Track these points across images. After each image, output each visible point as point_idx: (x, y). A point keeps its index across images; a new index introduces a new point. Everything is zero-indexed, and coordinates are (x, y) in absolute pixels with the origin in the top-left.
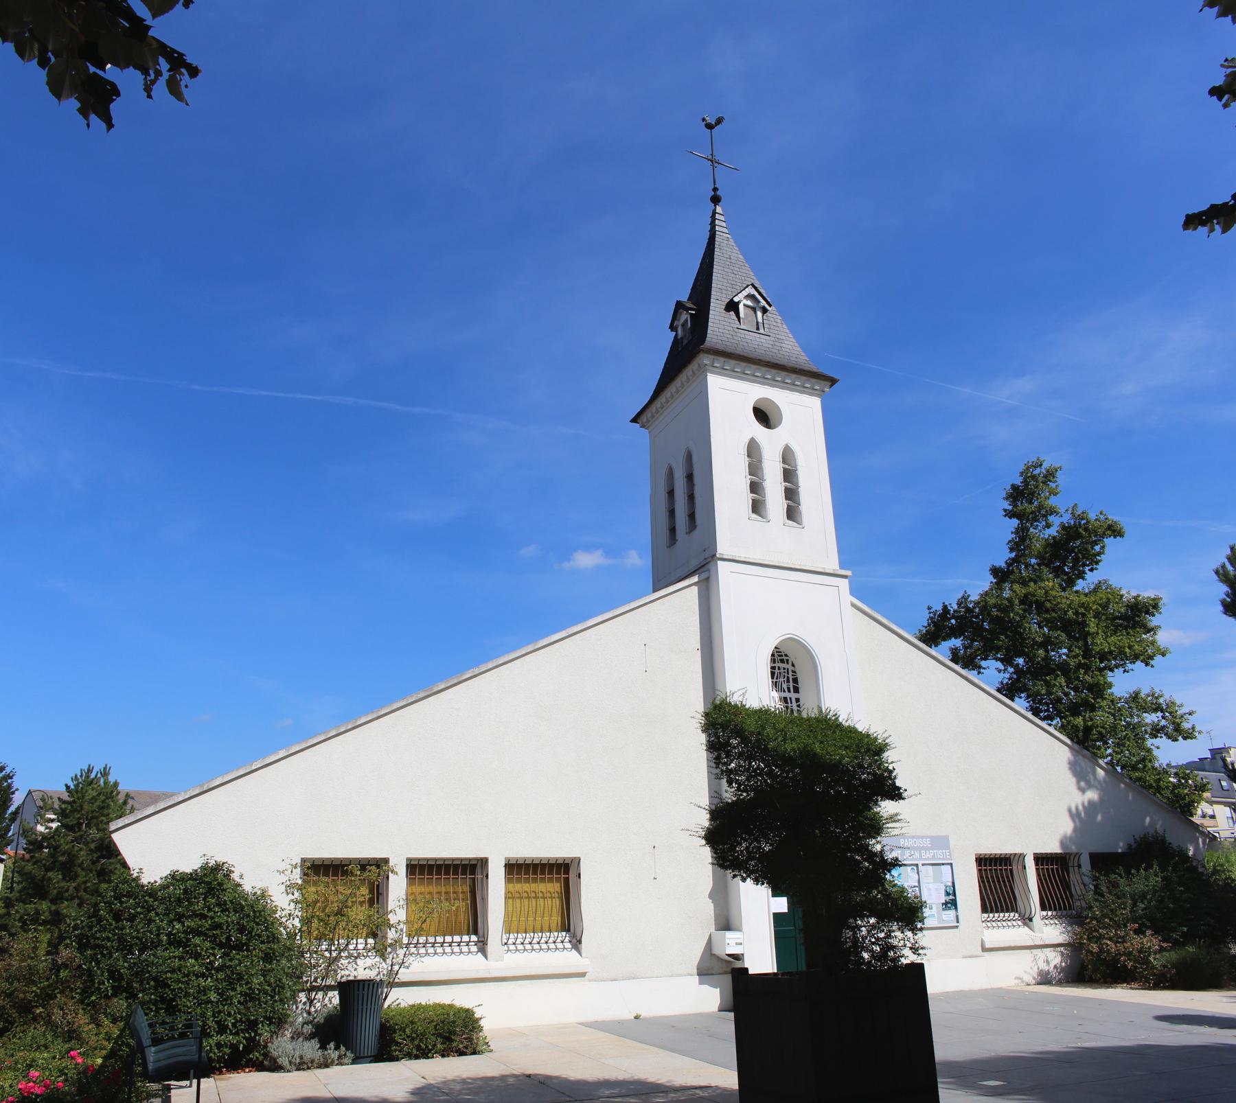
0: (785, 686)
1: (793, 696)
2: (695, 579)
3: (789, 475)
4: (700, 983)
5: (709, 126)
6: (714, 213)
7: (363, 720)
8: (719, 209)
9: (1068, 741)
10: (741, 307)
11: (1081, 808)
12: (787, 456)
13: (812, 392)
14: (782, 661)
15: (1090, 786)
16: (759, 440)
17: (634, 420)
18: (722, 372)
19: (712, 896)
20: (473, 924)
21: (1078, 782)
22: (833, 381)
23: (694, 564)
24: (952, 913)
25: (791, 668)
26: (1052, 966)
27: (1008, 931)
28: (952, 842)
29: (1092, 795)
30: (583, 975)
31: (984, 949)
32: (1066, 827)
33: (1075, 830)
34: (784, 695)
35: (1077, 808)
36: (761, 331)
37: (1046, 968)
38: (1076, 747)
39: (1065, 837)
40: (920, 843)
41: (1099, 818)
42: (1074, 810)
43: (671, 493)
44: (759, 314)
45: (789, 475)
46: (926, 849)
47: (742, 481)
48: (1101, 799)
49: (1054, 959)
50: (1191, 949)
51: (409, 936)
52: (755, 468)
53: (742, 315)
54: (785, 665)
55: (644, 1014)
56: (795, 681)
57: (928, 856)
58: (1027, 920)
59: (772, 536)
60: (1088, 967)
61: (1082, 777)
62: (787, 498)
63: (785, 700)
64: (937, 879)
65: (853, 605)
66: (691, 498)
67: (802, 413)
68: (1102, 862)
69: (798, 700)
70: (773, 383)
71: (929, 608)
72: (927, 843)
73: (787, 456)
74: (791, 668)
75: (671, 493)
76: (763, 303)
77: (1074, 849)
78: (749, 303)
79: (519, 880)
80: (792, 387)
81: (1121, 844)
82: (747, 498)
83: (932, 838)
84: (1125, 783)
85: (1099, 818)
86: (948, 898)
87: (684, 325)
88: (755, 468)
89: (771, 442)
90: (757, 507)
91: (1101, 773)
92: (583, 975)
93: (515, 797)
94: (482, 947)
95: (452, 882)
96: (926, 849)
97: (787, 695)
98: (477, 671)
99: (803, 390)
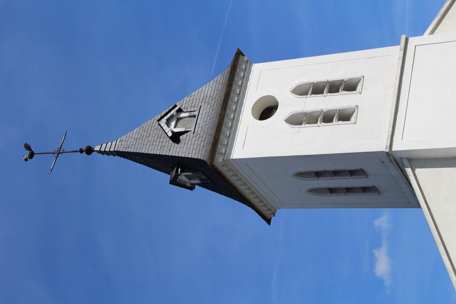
2: (409, 171)
3: (317, 89)
5: (32, 155)
6: (100, 152)
8: (97, 148)
10: (176, 130)
12: (301, 91)
13: (248, 71)
17: (269, 221)
18: (229, 146)
22: (239, 54)
23: (395, 172)
36: (196, 113)
43: (332, 191)
44: (183, 115)
45: (317, 89)
47: (323, 129)
52: (310, 119)
53: (183, 130)
62: (337, 91)
66: (336, 173)
67: (266, 79)
70: (239, 103)
73: (301, 91)
75: (332, 191)
76: (173, 112)
78: (173, 124)
80: (244, 87)
87: (190, 178)
88: (310, 119)
89: (289, 104)
90: (345, 116)
99: (246, 79)
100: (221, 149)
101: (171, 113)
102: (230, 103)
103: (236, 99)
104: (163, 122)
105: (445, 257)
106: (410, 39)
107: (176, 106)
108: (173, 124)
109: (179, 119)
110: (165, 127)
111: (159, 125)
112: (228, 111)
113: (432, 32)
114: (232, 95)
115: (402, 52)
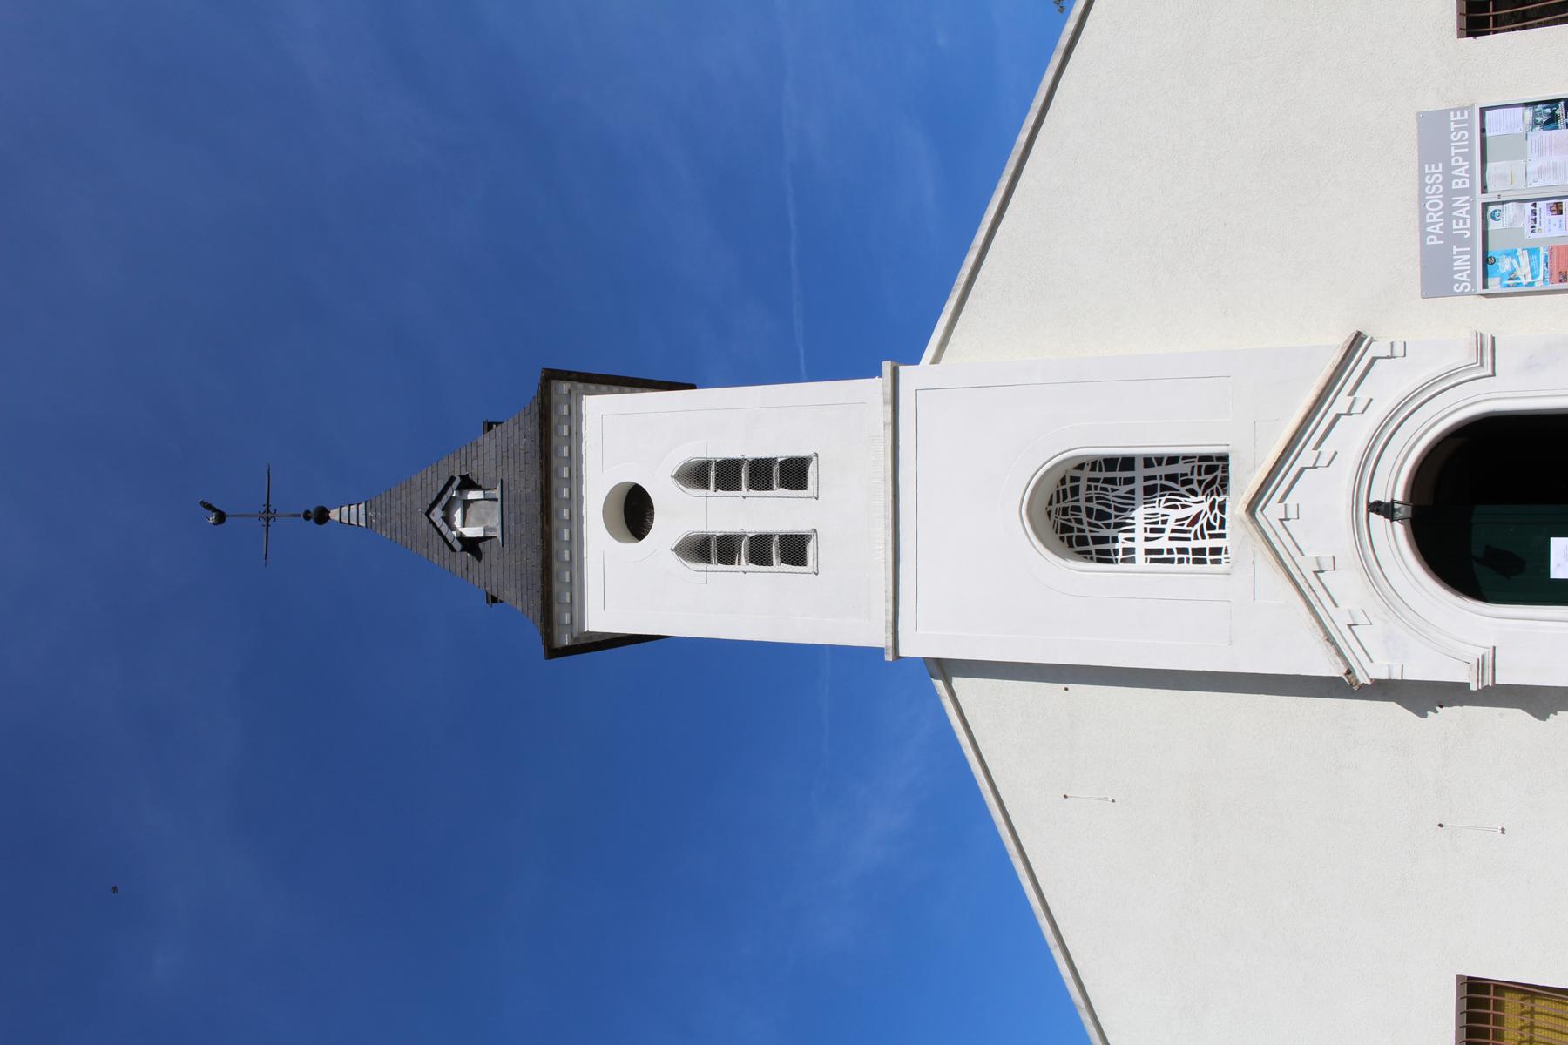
0: (1123, 490)
1: (1140, 472)
5: (221, 517)
12: (696, 475)
13: (575, 418)
14: (1075, 491)
16: (675, 540)
25: (1086, 474)
28: (1431, 104)
34: (1139, 494)
40: (1435, 193)
44: (472, 495)
46: (1448, 177)
47: (744, 577)
54: (1083, 484)
57: (1465, 172)
63: (1149, 491)
64: (1517, 149)
65: (936, 360)
67: (622, 438)
69: (1148, 462)
72: (1435, 171)
73: (696, 475)
74: (1086, 474)
80: (575, 479)
82: (779, 573)
90: (794, 549)
96: (1448, 177)
97: (1139, 486)
99: (575, 437)
102: (555, 504)
103: (566, 491)
105: (1023, 137)
106: (903, 369)
108: (458, 515)
111: (432, 522)
115: (890, 408)
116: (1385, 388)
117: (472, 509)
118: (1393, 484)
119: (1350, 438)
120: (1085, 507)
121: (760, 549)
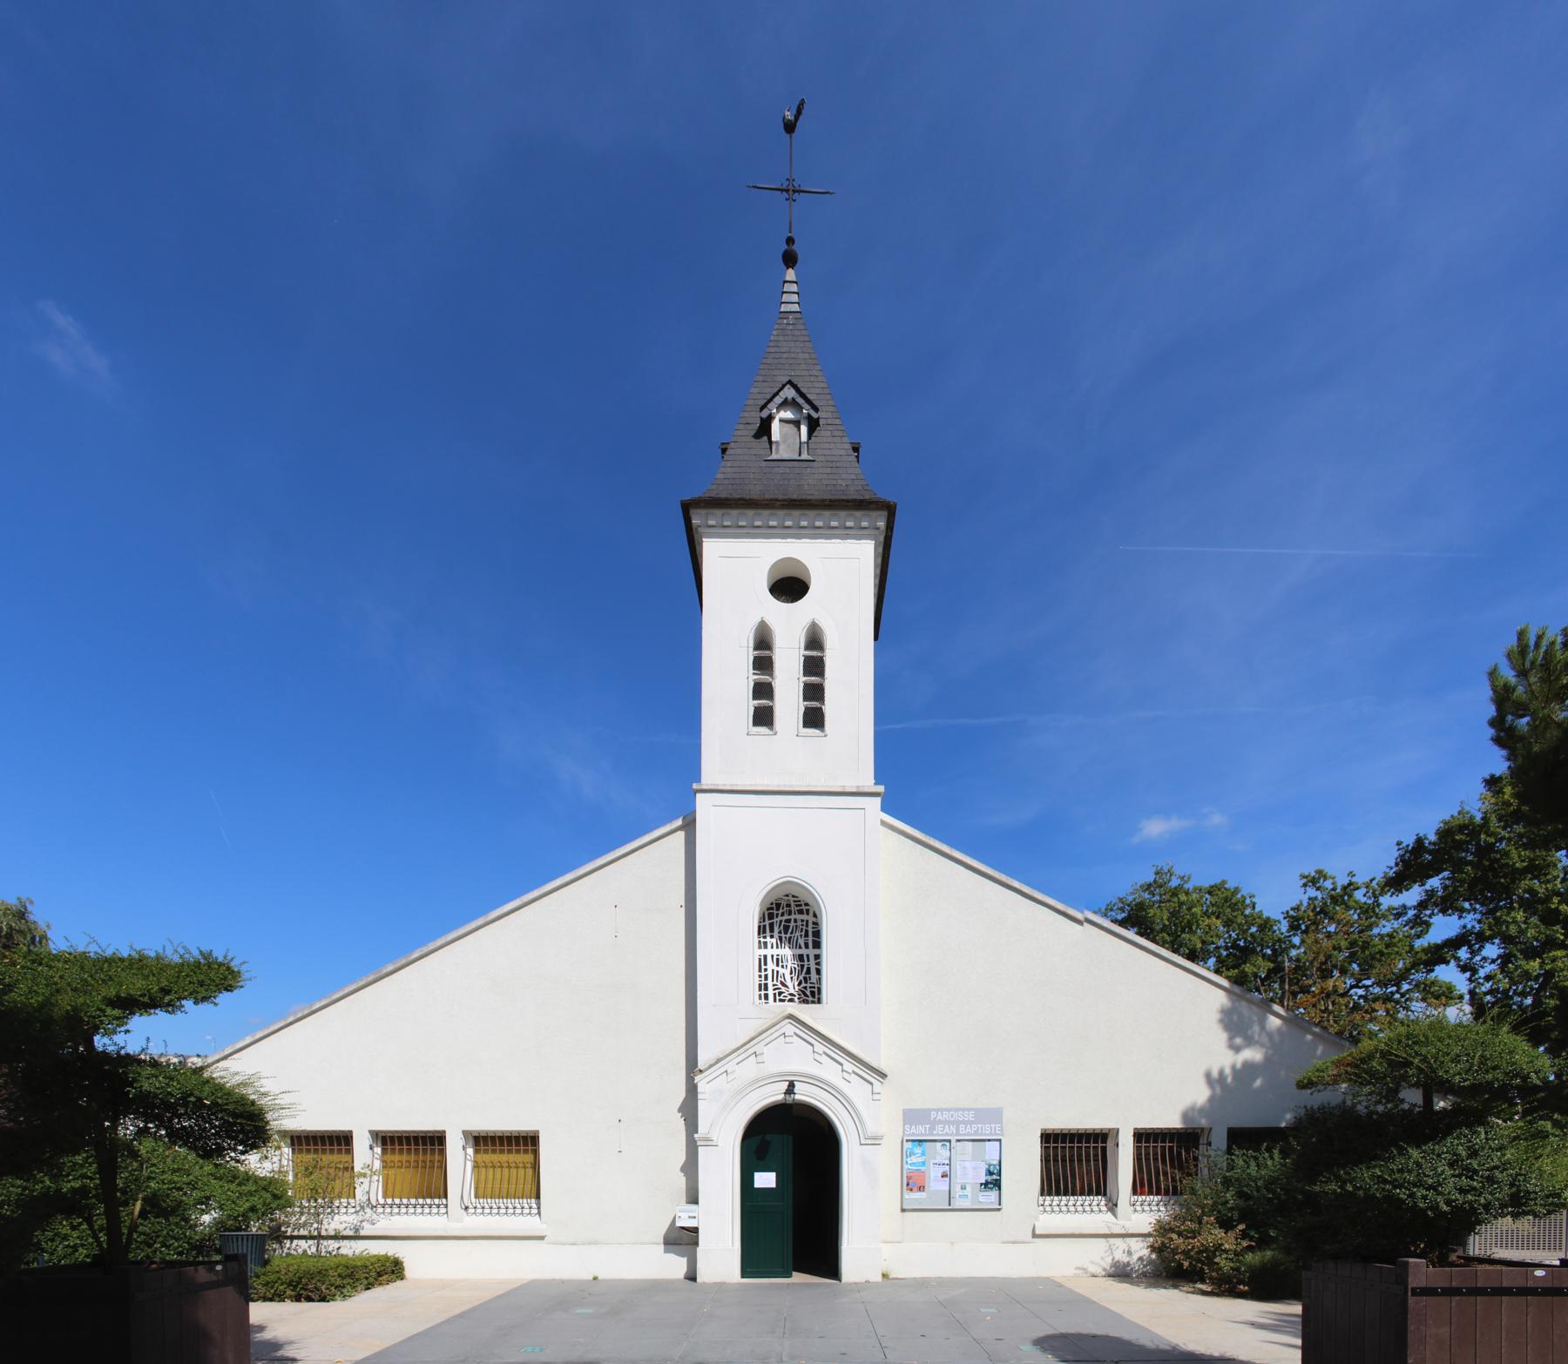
0: (802, 942)
1: (812, 952)
3: (814, 666)
4: (666, 1251)
7: (318, 1006)
9: (1225, 983)
11: (1228, 1071)
12: (814, 641)
13: (857, 533)
14: (801, 912)
15: (1250, 1042)
18: (724, 532)
19: (683, 1169)
20: (434, 1188)
21: (1231, 1039)
24: (993, 1194)
25: (811, 919)
26: (1135, 1257)
27: (1083, 1214)
28: (1007, 1115)
29: (1253, 1054)
30: (542, 1238)
31: (1035, 1235)
32: (1200, 1094)
33: (1211, 1099)
35: (1221, 1072)
37: (1125, 1259)
38: (1237, 989)
39: (1192, 1108)
41: (1258, 1083)
42: (1215, 1074)
44: (804, 429)
45: (814, 666)
47: (746, 677)
48: (1267, 1059)
49: (1140, 1250)
50: (1269, 1253)
51: (385, 1196)
54: (804, 917)
55: (897, 1272)
56: (817, 934)
57: (968, 1131)
58: (1112, 1207)
59: (788, 750)
60: (1174, 1266)
61: (1234, 1026)
65: (883, 823)
67: (843, 567)
68: (1240, 1138)
69: (817, 957)
70: (797, 532)
71: (1399, 844)
72: (970, 1116)
73: (814, 641)
74: (811, 919)
77: (1203, 1123)
79: (486, 1152)
80: (827, 533)
81: (1288, 1116)
83: (977, 1110)
84: (1314, 1034)
85: (1258, 1083)
86: (989, 1178)
90: (763, 717)
91: (1274, 1022)
92: (542, 1238)
93: (485, 1073)
94: (1112, 1207)
95: (415, 1153)
97: (804, 951)
98: (425, 950)
100: (714, 517)
101: (806, 406)
104: (789, 393)
106: (878, 800)
107: (816, 409)
109: (797, 424)
110: (778, 400)
112: (781, 513)
113: (883, 823)
114: (811, 513)
116: (856, 1090)
117: (791, 428)
118: (804, 1094)
119: (829, 1071)
120: (791, 917)
121: (763, 690)
